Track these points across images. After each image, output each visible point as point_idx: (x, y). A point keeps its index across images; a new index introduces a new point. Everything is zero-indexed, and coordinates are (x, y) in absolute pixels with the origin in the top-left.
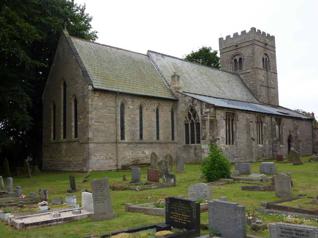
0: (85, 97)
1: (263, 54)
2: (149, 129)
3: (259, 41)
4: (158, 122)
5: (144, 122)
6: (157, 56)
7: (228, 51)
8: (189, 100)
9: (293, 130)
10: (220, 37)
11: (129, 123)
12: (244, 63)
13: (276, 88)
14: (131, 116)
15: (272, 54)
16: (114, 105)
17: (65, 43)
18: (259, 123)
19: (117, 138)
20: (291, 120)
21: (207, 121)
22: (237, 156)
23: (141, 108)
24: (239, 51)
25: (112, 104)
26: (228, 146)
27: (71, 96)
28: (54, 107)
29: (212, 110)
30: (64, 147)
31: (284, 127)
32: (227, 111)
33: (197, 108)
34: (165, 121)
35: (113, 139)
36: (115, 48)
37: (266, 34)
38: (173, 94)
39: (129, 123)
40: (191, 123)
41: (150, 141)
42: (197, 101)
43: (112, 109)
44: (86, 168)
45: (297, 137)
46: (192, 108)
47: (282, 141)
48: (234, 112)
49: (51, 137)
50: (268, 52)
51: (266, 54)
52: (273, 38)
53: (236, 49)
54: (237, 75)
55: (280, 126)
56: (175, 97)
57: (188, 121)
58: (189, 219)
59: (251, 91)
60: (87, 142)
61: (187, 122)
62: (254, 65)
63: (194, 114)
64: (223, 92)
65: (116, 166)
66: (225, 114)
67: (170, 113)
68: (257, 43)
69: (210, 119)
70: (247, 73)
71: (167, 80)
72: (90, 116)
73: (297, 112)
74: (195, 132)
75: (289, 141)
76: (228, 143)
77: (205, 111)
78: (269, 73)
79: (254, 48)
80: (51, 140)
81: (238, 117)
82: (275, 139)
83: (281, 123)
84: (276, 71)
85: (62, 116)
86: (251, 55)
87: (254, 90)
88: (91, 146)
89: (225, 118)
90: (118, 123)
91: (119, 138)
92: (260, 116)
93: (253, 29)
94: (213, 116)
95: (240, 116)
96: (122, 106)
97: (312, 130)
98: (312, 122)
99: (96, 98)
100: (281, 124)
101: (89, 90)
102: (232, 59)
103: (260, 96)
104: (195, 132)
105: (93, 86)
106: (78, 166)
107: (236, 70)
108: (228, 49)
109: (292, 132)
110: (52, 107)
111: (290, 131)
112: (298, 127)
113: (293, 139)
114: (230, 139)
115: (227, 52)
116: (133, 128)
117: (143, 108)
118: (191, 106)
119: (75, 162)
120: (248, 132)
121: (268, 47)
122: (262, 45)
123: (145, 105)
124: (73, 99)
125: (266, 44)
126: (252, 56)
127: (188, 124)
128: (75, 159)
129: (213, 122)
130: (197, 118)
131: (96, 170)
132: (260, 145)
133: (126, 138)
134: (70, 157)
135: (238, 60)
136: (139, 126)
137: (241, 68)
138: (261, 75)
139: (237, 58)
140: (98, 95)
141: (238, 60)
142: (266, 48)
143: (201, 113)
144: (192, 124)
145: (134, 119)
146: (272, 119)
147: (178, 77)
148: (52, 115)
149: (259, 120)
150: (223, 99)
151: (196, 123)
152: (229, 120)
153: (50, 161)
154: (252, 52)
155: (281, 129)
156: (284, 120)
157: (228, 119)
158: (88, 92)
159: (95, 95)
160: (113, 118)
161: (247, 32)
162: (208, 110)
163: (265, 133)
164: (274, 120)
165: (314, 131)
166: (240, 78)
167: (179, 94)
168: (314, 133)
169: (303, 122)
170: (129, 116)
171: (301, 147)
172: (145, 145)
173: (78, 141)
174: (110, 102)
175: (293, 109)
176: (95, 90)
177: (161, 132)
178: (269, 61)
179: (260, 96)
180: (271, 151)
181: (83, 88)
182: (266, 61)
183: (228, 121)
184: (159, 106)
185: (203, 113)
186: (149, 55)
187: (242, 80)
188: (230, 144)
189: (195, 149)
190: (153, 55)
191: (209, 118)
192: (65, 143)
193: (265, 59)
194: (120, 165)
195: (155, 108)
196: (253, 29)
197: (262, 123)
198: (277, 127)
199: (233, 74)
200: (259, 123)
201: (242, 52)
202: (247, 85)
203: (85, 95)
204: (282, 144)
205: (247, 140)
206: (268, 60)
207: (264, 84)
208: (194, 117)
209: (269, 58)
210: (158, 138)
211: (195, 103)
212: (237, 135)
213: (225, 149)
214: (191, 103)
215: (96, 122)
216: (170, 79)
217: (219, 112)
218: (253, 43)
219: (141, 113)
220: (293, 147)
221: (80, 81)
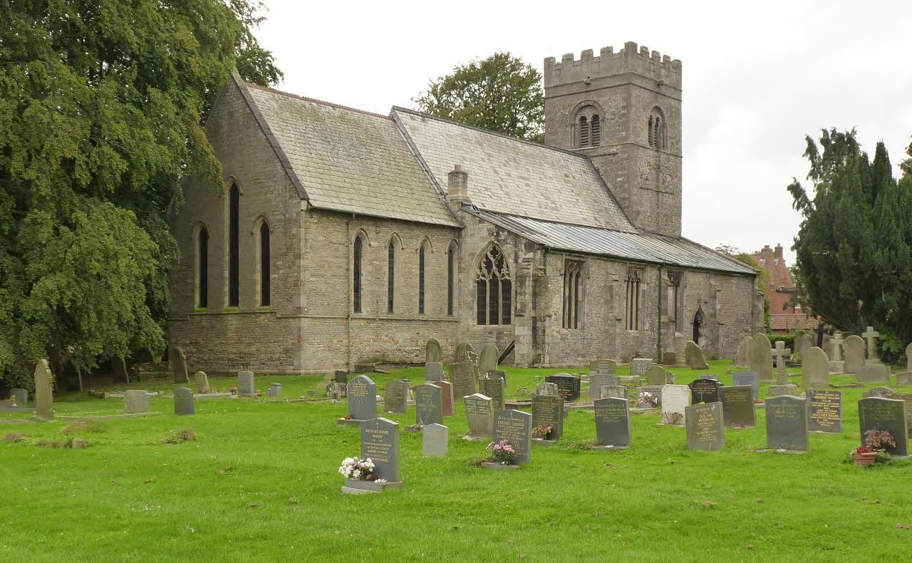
0: (290, 222)
1: (651, 108)
2: (405, 290)
3: (642, 77)
4: (423, 277)
5: (396, 275)
6: (413, 119)
7: (566, 93)
8: (489, 230)
9: (707, 299)
10: (549, 56)
11: (370, 278)
12: (605, 129)
13: (676, 192)
14: (375, 262)
15: (672, 107)
16: (344, 240)
17: (234, 99)
18: (632, 282)
19: (348, 307)
20: (704, 275)
21: (527, 278)
22: (582, 352)
23: (391, 246)
24: (593, 97)
25: (341, 237)
26: (565, 331)
27: (254, 219)
28: (204, 236)
29: (539, 254)
30: (233, 323)
31: (687, 292)
32: (569, 258)
33: (507, 249)
34: (437, 274)
35: (341, 312)
36: (329, 104)
37: (662, 56)
38: (452, 216)
39: (370, 278)
40: (490, 280)
41: (407, 316)
42: (506, 233)
43: (340, 247)
44: (292, 367)
45: (714, 315)
46: (494, 248)
47: (681, 323)
48: (582, 259)
49: (194, 303)
50: (663, 103)
51: (657, 108)
52: (677, 66)
53: (587, 91)
54: (585, 157)
55: (679, 289)
56: (457, 221)
57: (484, 276)
58: (570, 393)
59: (618, 199)
60: (297, 313)
61: (483, 279)
62: (626, 138)
63: (499, 262)
64: (554, 206)
65: (345, 366)
66: (564, 263)
67: (446, 257)
68: (638, 82)
69: (534, 276)
70: (609, 155)
71: (437, 180)
72: (302, 262)
73: (723, 254)
74: (501, 301)
75: (696, 324)
76: (566, 326)
77: (524, 256)
78: (663, 157)
79: (630, 95)
80: (194, 307)
81: (588, 270)
82: (664, 319)
83: (681, 283)
84: (680, 149)
85: (227, 258)
86: (623, 112)
87: (624, 199)
88: (305, 323)
89: (563, 272)
90: (350, 277)
91: (352, 308)
92: (635, 267)
93: (631, 46)
94: (539, 267)
95: (593, 267)
96: (358, 242)
97: (753, 300)
98: (753, 281)
99: (313, 226)
100: (681, 286)
101: (302, 210)
102: (576, 115)
103: (638, 213)
104: (501, 301)
105: (308, 201)
106: (272, 362)
107: (584, 143)
108: (565, 88)
109: (706, 302)
110: (197, 235)
111: (699, 301)
112: (718, 293)
113: (706, 320)
114: (572, 317)
115: (564, 97)
116: (377, 288)
117: (395, 246)
118: (493, 242)
119: (262, 355)
120: (609, 302)
121: (663, 90)
122: (650, 86)
123: (399, 240)
124: (259, 224)
125: (659, 84)
126: (624, 115)
127: (485, 281)
128: (263, 349)
129: (539, 283)
130: (504, 271)
131: (312, 371)
132: (631, 331)
133: (363, 309)
134: (249, 344)
135: (589, 120)
136: (387, 284)
137: (595, 141)
138: (645, 161)
139: (589, 114)
140: (316, 221)
141: (589, 120)
142: (658, 93)
143: (516, 261)
144: (494, 282)
145: (378, 269)
146: (662, 273)
147: (465, 174)
148: (197, 253)
149: (633, 276)
150: (554, 223)
151: (502, 281)
152: (571, 275)
153: (193, 354)
154: (625, 104)
155: (679, 296)
156: (690, 278)
157: (568, 275)
158: (298, 214)
159: (312, 220)
160: (341, 267)
161: (616, 51)
162: (530, 255)
163: (644, 306)
164: (665, 277)
165: (756, 303)
166: (592, 164)
167: (467, 215)
168: (756, 306)
169: (732, 281)
170: (371, 264)
171: (721, 339)
172: (398, 324)
173: (273, 313)
174: (339, 235)
175: (713, 247)
176: (313, 210)
177: (427, 297)
178: (664, 126)
179: (638, 213)
180: (655, 346)
181: (285, 203)
182: (657, 125)
183: (567, 279)
184: (425, 240)
185: (520, 261)
186: (395, 119)
187: (597, 171)
188: (569, 327)
189: (500, 335)
190: (404, 117)
191: (531, 271)
192: (235, 317)
193: (655, 121)
194: (354, 360)
195: (418, 247)
196: (631, 46)
197: (638, 283)
198: (671, 292)
199: (574, 154)
200: (632, 282)
201: (601, 100)
202: (608, 185)
203: (290, 220)
204: (680, 331)
205: (606, 319)
206: (661, 122)
207: (651, 184)
208: (500, 267)
209: (663, 118)
210: (421, 310)
211: (503, 238)
212: (586, 308)
213: (559, 337)
214: (493, 237)
215: (313, 275)
216: (446, 179)
217: (551, 259)
218: (626, 82)
219: (391, 256)
220: (703, 338)
221: (279, 189)
